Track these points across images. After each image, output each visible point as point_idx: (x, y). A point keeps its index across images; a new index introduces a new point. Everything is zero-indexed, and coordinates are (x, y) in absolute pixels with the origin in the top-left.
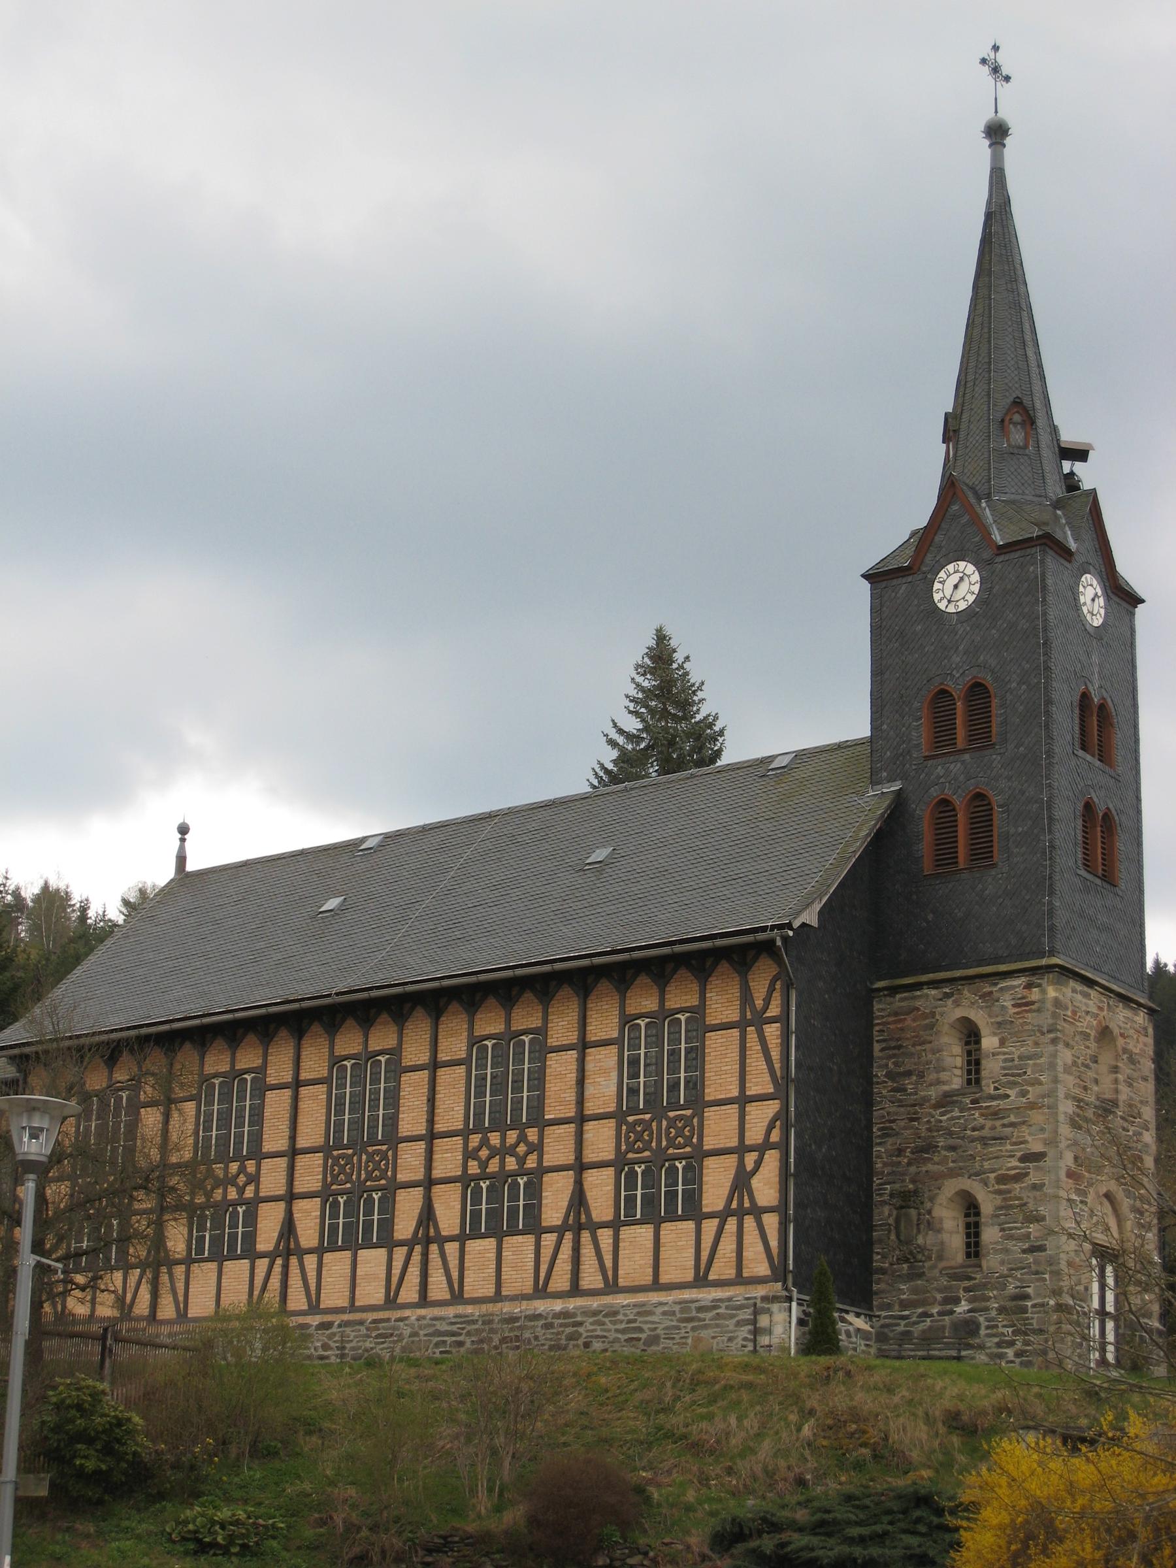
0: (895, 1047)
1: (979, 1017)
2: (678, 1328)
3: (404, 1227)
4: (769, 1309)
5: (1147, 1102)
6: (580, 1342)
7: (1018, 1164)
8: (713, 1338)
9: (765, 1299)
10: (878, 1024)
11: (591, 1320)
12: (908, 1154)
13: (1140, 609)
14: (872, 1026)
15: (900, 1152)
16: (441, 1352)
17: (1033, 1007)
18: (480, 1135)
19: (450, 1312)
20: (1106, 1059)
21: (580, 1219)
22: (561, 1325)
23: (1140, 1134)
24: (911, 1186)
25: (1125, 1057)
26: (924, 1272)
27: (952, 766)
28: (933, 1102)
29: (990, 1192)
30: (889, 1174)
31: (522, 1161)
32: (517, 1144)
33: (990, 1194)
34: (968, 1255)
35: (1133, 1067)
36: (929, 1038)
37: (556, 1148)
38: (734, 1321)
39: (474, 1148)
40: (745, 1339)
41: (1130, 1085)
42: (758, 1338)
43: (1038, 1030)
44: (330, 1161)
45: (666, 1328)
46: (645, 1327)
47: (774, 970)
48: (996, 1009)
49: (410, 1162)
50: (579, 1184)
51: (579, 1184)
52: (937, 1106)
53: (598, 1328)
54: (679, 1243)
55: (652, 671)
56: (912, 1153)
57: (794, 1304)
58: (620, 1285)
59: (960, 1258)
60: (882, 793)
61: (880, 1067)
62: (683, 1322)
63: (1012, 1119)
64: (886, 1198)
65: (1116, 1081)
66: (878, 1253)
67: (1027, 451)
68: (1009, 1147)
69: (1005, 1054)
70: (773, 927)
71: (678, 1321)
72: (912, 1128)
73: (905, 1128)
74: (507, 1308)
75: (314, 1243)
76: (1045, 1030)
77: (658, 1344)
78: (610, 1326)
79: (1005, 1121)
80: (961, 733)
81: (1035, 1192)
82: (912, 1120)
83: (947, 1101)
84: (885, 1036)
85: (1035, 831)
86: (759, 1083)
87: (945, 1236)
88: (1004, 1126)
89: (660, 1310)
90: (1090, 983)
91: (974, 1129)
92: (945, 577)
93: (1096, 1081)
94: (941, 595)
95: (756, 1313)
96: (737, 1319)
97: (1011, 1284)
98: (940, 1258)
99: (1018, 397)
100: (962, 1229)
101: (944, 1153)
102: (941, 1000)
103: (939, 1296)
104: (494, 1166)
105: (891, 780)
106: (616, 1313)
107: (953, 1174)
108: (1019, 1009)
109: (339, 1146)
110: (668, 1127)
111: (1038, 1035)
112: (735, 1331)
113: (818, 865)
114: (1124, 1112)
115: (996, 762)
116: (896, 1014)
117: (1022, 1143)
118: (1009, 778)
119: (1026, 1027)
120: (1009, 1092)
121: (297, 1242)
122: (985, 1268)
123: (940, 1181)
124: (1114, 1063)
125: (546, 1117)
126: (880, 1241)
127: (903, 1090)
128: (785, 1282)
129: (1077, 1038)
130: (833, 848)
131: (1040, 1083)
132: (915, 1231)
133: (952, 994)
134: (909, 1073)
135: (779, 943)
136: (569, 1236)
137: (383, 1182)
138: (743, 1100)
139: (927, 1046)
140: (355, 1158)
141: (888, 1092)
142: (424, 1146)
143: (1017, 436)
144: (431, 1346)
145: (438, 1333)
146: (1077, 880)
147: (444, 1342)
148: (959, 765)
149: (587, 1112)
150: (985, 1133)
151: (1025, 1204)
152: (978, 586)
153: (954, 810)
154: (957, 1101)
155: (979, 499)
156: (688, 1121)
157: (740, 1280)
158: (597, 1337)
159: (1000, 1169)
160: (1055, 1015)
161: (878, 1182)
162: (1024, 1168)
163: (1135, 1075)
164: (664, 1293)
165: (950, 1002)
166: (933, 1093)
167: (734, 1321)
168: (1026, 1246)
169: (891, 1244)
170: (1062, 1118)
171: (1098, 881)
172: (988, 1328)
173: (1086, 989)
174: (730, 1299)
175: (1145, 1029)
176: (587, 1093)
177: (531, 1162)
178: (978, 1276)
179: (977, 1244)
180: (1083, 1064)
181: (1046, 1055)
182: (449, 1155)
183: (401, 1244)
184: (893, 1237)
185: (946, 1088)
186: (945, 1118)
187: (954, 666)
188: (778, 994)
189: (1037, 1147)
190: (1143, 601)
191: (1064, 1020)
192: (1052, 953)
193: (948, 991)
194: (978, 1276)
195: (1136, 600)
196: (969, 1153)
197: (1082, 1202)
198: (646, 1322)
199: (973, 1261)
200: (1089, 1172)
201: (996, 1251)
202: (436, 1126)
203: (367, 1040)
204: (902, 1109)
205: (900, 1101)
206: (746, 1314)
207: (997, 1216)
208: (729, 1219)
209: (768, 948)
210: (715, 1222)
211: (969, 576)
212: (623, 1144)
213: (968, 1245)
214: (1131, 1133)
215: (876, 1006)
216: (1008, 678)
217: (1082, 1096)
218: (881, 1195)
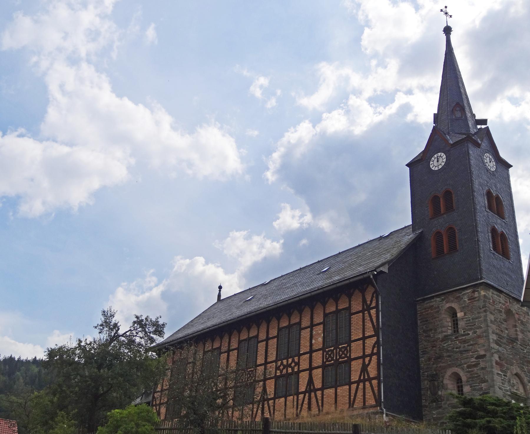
1: (454, 305)
10: (419, 313)
12: (432, 360)
13: (511, 170)
15: (430, 359)
17: (476, 299)
20: (511, 322)
21: (311, 388)
25: (519, 322)
26: (442, 406)
27: (440, 220)
28: (441, 339)
33: (465, 373)
41: (523, 333)
52: (442, 341)
63: (472, 343)
65: (516, 331)
67: (462, 118)
68: (471, 354)
79: (469, 344)
82: (433, 347)
83: (446, 338)
88: (468, 346)
90: (501, 292)
91: (457, 348)
93: (507, 329)
94: (433, 165)
102: (441, 301)
105: (419, 229)
107: (450, 366)
114: (521, 343)
117: (476, 352)
124: (514, 324)
127: (429, 336)
128: (380, 406)
129: (496, 311)
131: (481, 328)
133: (445, 299)
134: (431, 330)
135: (372, 277)
138: (364, 338)
139: (437, 319)
143: (458, 114)
150: (461, 349)
151: (479, 376)
153: (442, 235)
155: (445, 135)
160: (484, 301)
162: (478, 361)
163: (525, 329)
165: (444, 302)
166: (440, 336)
170: (491, 341)
180: (500, 322)
181: (482, 316)
186: (446, 345)
188: (375, 298)
189: (482, 353)
190: (512, 166)
191: (489, 303)
192: (481, 279)
193: (443, 298)
200: (507, 364)
208: (360, 383)
210: (355, 385)
214: (525, 352)
215: (418, 307)
217: (500, 333)
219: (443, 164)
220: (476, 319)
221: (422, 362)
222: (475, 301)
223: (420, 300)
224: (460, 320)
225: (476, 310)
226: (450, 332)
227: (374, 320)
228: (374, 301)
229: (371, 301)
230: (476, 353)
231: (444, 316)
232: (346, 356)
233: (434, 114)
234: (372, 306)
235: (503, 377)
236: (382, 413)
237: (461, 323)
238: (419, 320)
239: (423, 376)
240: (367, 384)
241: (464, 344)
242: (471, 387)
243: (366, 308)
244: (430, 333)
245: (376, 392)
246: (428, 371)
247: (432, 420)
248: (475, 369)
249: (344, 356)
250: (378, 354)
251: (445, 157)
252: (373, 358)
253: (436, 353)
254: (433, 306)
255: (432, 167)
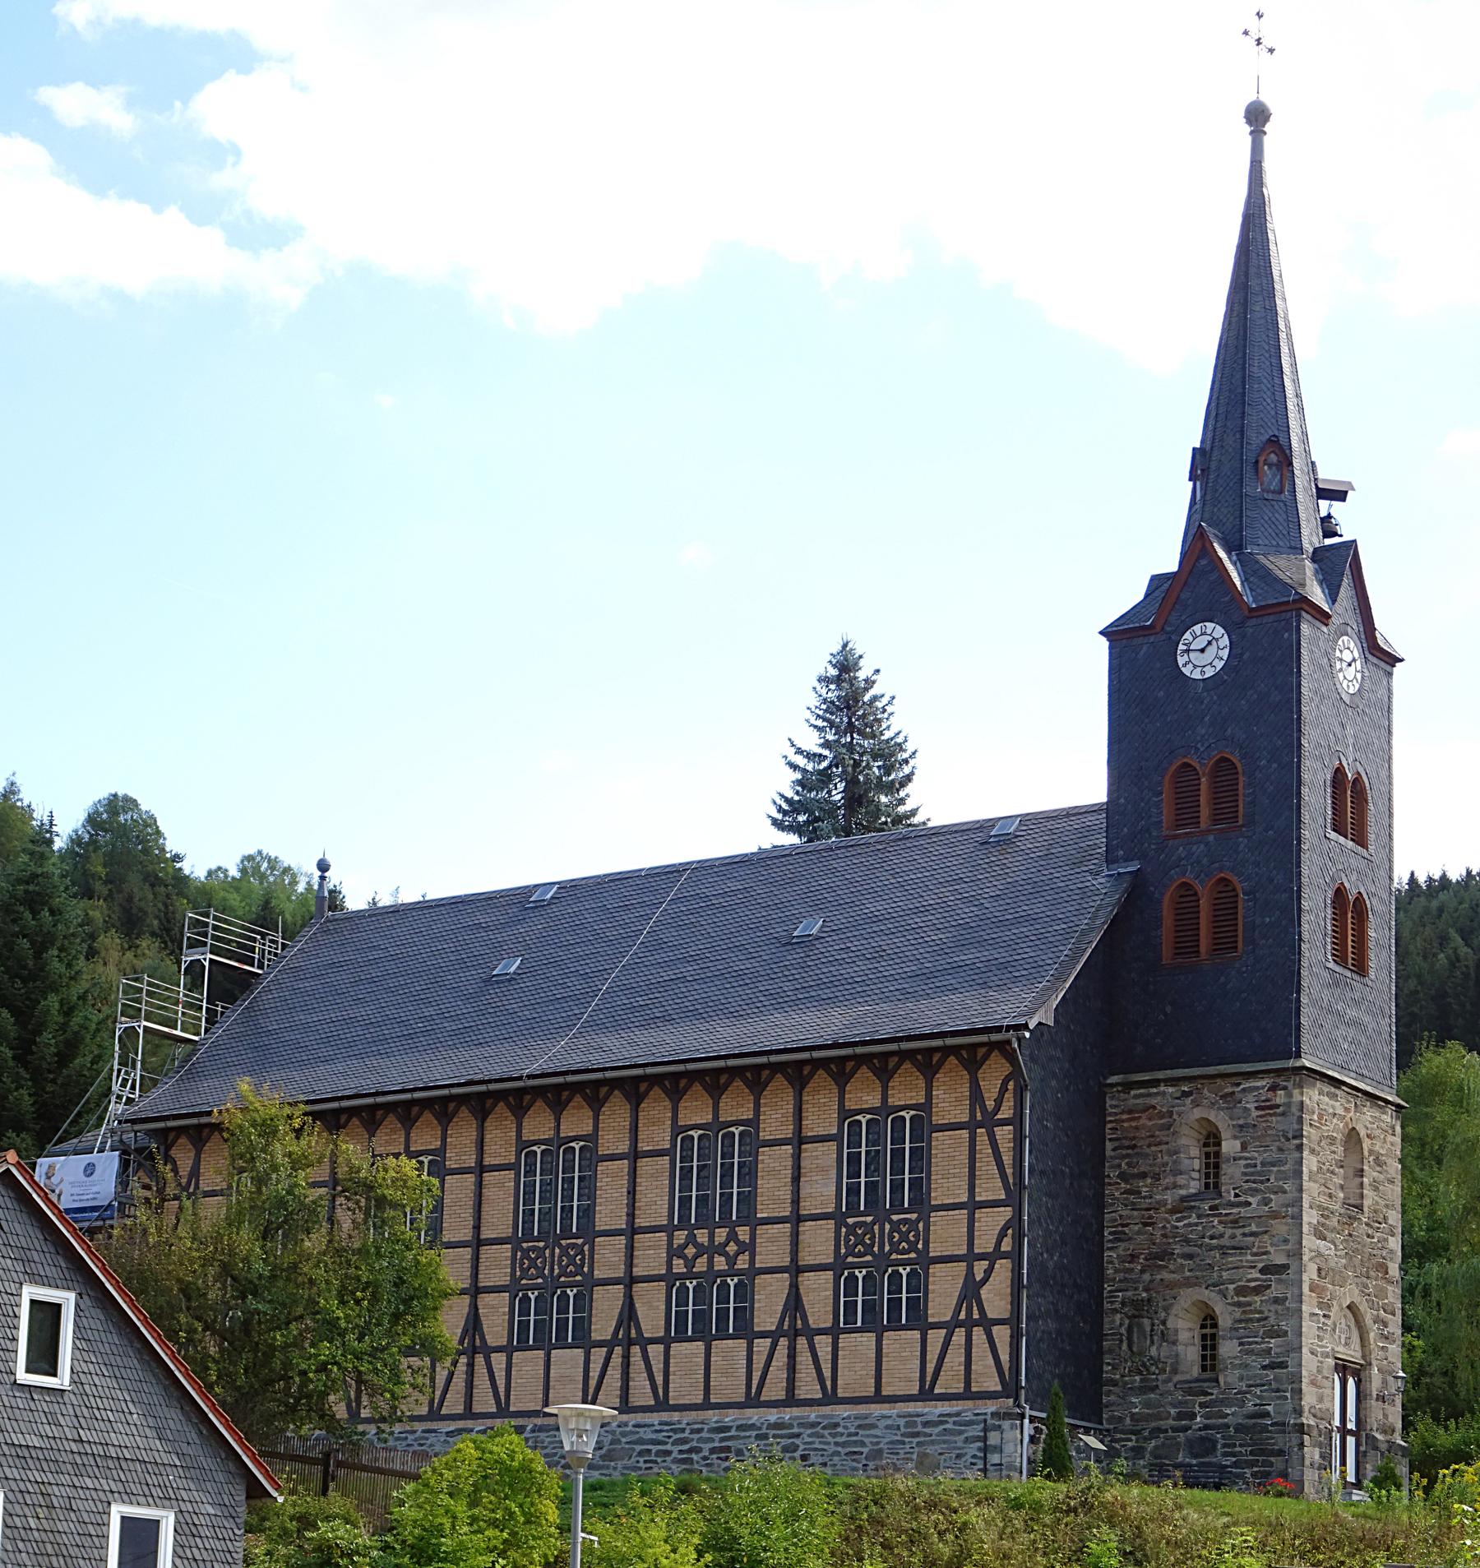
0: (1130, 1147)
1: (1220, 1119)
2: (903, 1443)
3: (603, 1325)
4: (1000, 1426)
5: (1393, 1205)
6: (797, 1454)
7: (1259, 1275)
8: (940, 1454)
9: (994, 1415)
10: (1111, 1122)
11: (809, 1431)
14: (1105, 1123)
15: (1133, 1258)
16: (645, 1462)
17: (1278, 1111)
18: (686, 1232)
19: (655, 1418)
22: (774, 1436)
23: (1386, 1240)
24: (1144, 1295)
27: (1195, 847)
28: (1169, 1207)
29: (1229, 1304)
30: (1120, 1281)
31: (732, 1261)
32: (737, 1254)
34: (1204, 1368)
35: (1378, 1169)
36: (1165, 1139)
37: (769, 1248)
38: (962, 1437)
39: (679, 1246)
40: (974, 1456)
41: (1376, 1189)
42: (988, 1455)
43: (1283, 1135)
44: (519, 1253)
45: (892, 1442)
46: (867, 1440)
47: (1007, 1069)
48: (1238, 1111)
49: (608, 1257)
50: (794, 1288)
51: (794, 1288)
52: (1173, 1211)
53: (817, 1440)
54: (903, 1354)
55: (838, 680)
56: (1146, 1259)
57: (1026, 1421)
58: (839, 1395)
59: (1196, 1371)
60: (1119, 874)
61: (1112, 1167)
62: (908, 1437)
63: (1254, 1228)
64: (1117, 1306)
66: (1109, 1364)
67: (1282, 495)
68: (1249, 1257)
69: (1246, 1159)
70: (1009, 1028)
71: (902, 1435)
72: (1146, 1233)
73: (1139, 1233)
74: (712, 1416)
75: (504, 1342)
76: (1290, 1136)
77: (881, 1459)
78: (830, 1439)
79: (1247, 1230)
80: (1205, 812)
81: (1276, 1306)
82: (1146, 1224)
83: (1184, 1206)
84: (1119, 1134)
85: (1284, 923)
86: (991, 1188)
87: (1180, 1348)
88: (1244, 1235)
89: (883, 1423)
91: (1212, 1238)
92: (1191, 639)
95: (985, 1430)
96: (966, 1435)
97: (1250, 1401)
98: (1175, 1371)
99: (1274, 436)
100: (1197, 1340)
101: (1179, 1260)
102: (1177, 1098)
103: (1173, 1411)
104: (701, 1265)
105: (1127, 859)
106: (836, 1425)
107: (1188, 1283)
108: (1263, 1113)
109: (528, 1235)
110: (891, 1232)
111: (1283, 1140)
112: (963, 1448)
113: (1051, 955)
115: (1242, 845)
116: (1130, 1112)
118: (1257, 864)
119: (1269, 1132)
120: (1250, 1199)
121: (483, 1339)
122: (1222, 1383)
123: (1175, 1291)
125: (758, 1216)
126: (1111, 1351)
128: (1017, 1398)
130: (1067, 936)
131: (1285, 1192)
132: (1148, 1342)
134: (1144, 1175)
136: (783, 1342)
137: (579, 1278)
138: (973, 1206)
139: (1164, 1147)
140: (547, 1251)
141: (1121, 1194)
142: (624, 1242)
144: (635, 1454)
145: (641, 1441)
146: (1326, 974)
147: (649, 1451)
148: (1202, 846)
149: (802, 1212)
150: (1225, 1241)
151: (1266, 1318)
152: (1227, 651)
154: (1194, 1207)
156: (913, 1225)
157: (968, 1395)
158: (816, 1449)
159: (1240, 1280)
161: (1109, 1288)
163: (1382, 1177)
164: (887, 1405)
165: (1188, 1101)
166: (1169, 1197)
167: (962, 1437)
168: (1267, 1362)
169: (1122, 1355)
170: (1305, 1228)
171: (1349, 974)
172: (1224, 1446)
173: (1333, 1090)
174: (958, 1414)
175: (1393, 1128)
176: (803, 1193)
177: (742, 1263)
178: (1215, 1392)
179: (1214, 1357)
182: (652, 1252)
183: (600, 1344)
184: (1125, 1346)
185: (1183, 1192)
186: (1181, 1224)
187: (1199, 738)
189: (1280, 1260)
191: (1311, 1124)
193: (1186, 1089)
194: (1215, 1392)
195: (1393, 660)
196: (1208, 1262)
197: (1324, 1316)
198: (868, 1436)
199: (1208, 1375)
201: (1234, 1366)
202: (637, 1221)
203: (559, 1125)
204: (1135, 1213)
205: (1133, 1204)
206: (976, 1431)
207: (1237, 1329)
208: (957, 1330)
209: (1003, 1047)
211: (1217, 640)
212: (843, 1247)
213: (1204, 1357)
215: (1109, 1102)
216: (1258, 754)
218: (1112, 1302)
219: (1220, 665)
220: (1274, 1166)
221: (1111, 1262)
222: (1275, 1114)
223: (1117, 1084)
224: (1228, 1160)
225: (1276, 1141)
226: (1194, 1187)
227: (1007, 1159)
228: (1008, 1104)
229: (999, 1102)
230: (1265, 1257)
231: (1183, 1141)
232: (913, 1247)
233: (1194, 449)
234: (998, 1117)
235: (1322, 1319)
236: (1022, 1416)
237: (1230, 1171)
238: (1110, 1140)
239: (1112, 1302)
240: (978, 1334)
241: (1232, 1228)
242: (1241, 1344)
243: (982, 1120)
244: (1141, 1184)
245: (1005, 1357)
246: (1127, 1290)
247: (1128, 1419)
248: (1256, 1298)
249: (906, 1247)
250: (1016, 1256)
251: (1228, 643)
252: (996, 1266)
253: (1154, 1244)
254: (1154, 1107)
255: (1185, 665)
